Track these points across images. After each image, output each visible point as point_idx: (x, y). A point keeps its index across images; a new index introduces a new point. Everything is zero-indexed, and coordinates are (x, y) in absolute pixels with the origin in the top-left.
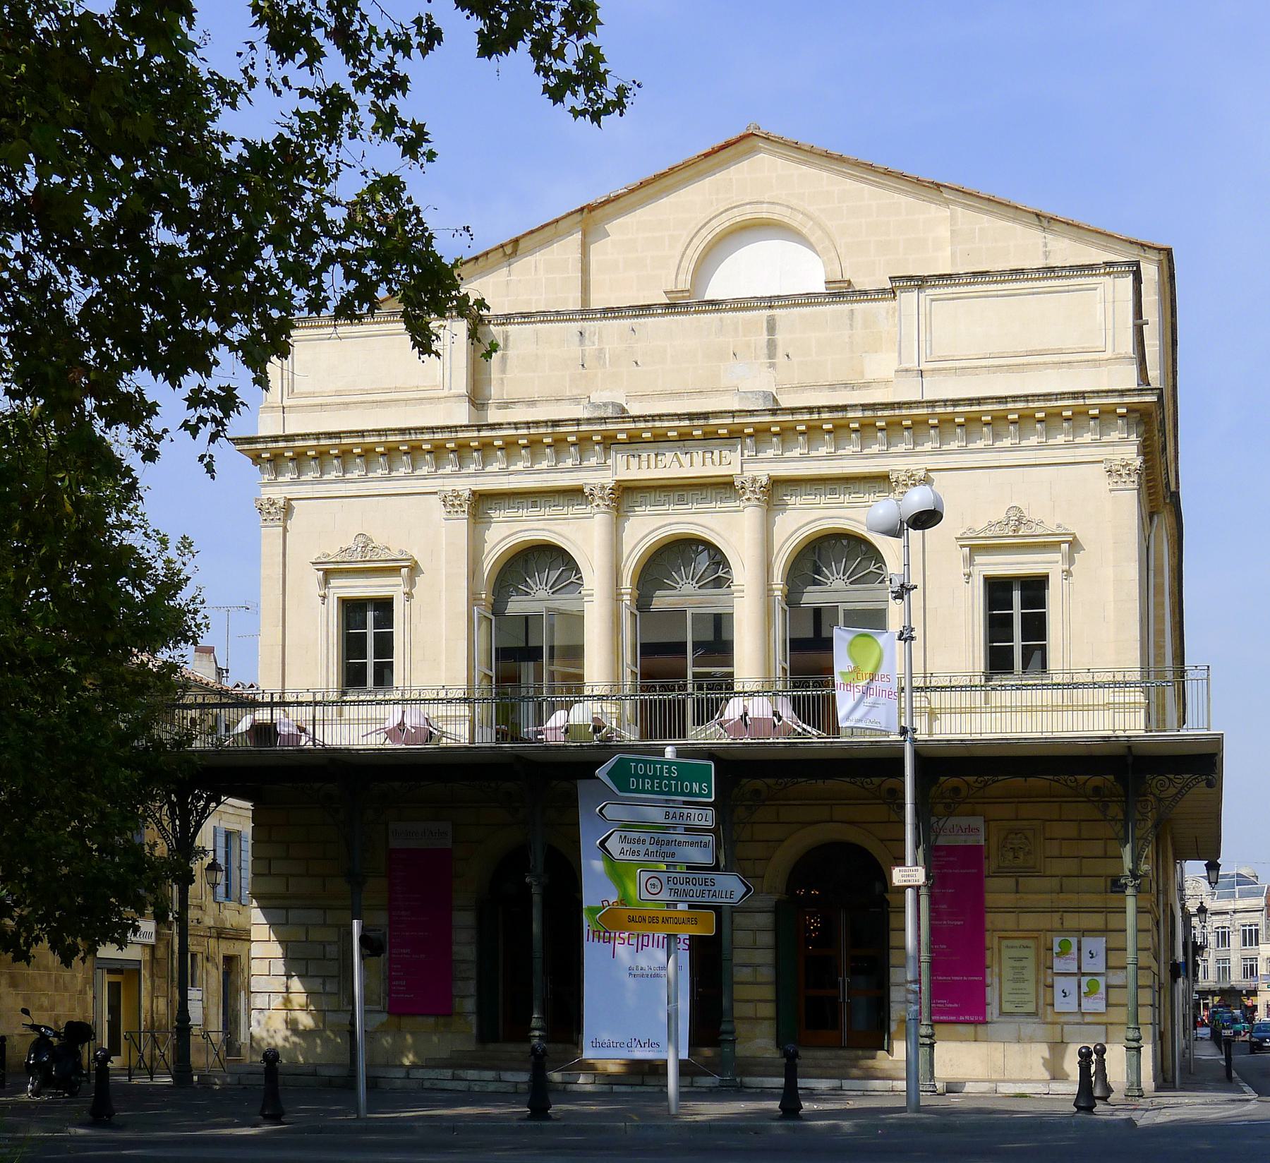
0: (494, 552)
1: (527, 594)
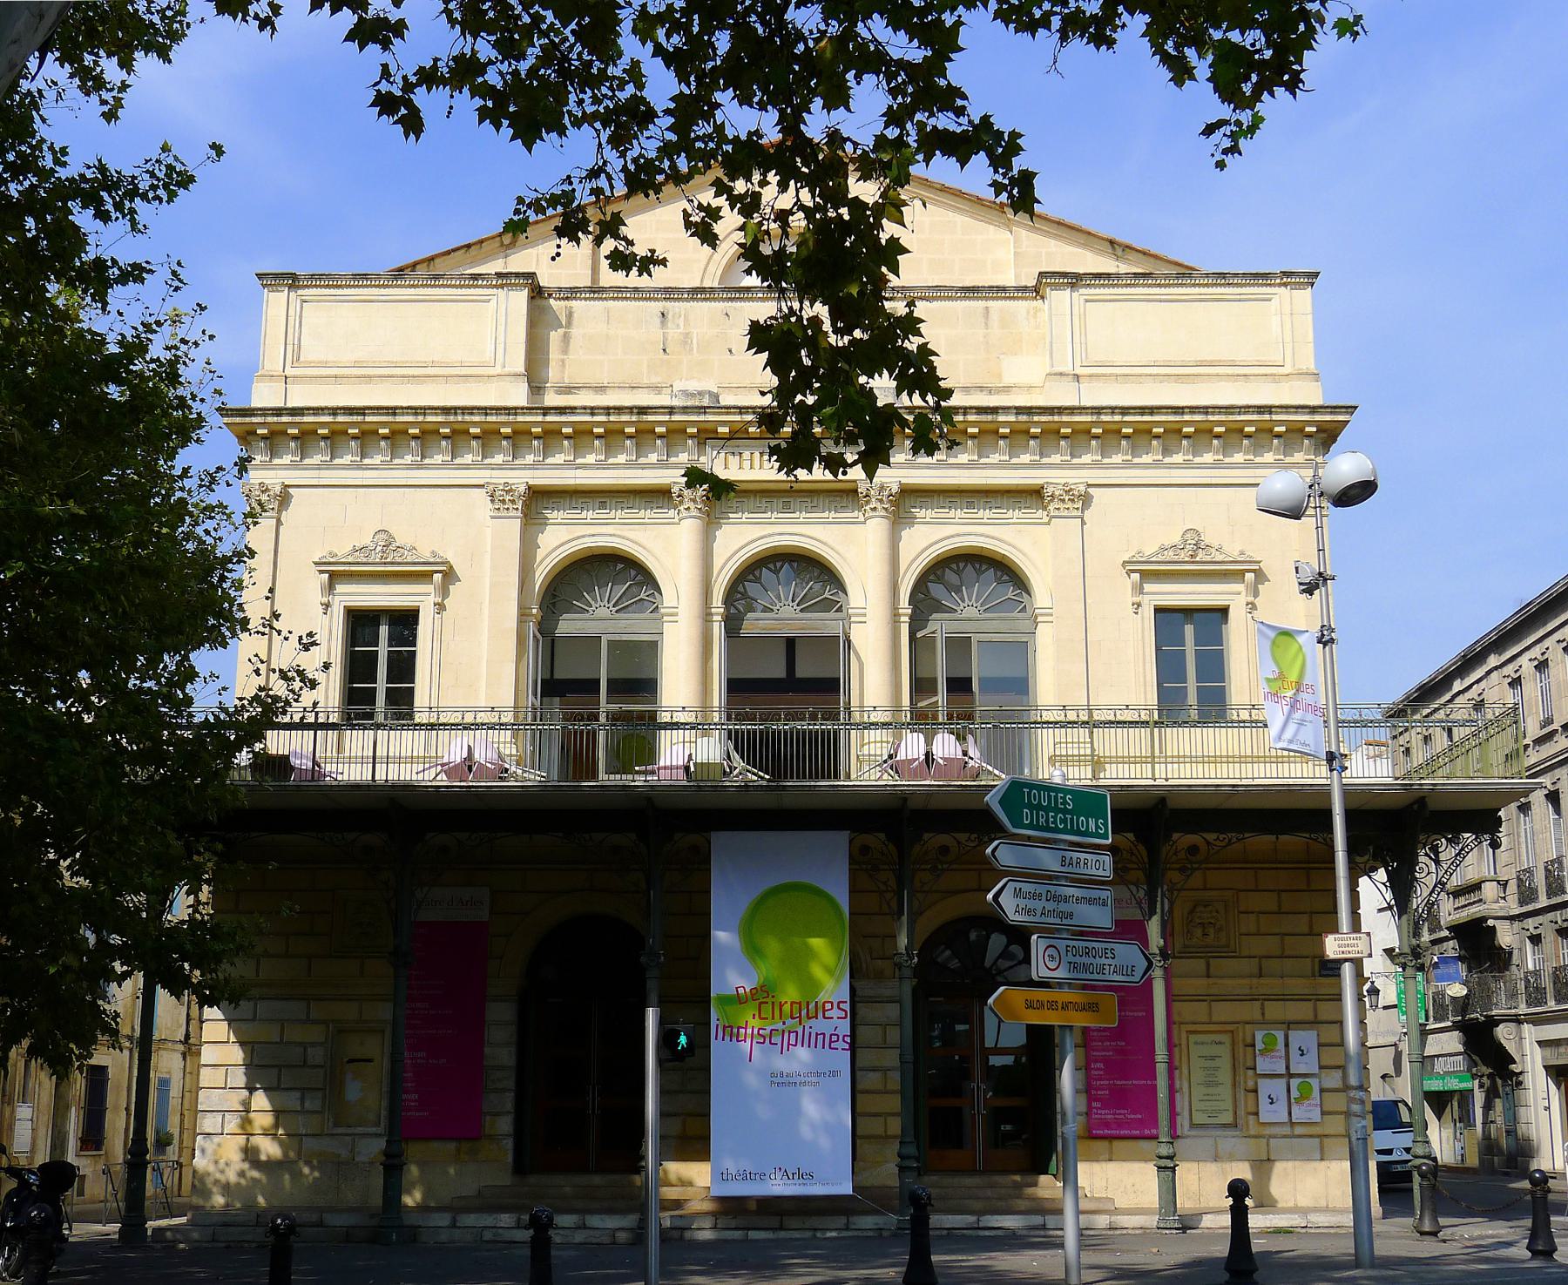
0: (548, 560)
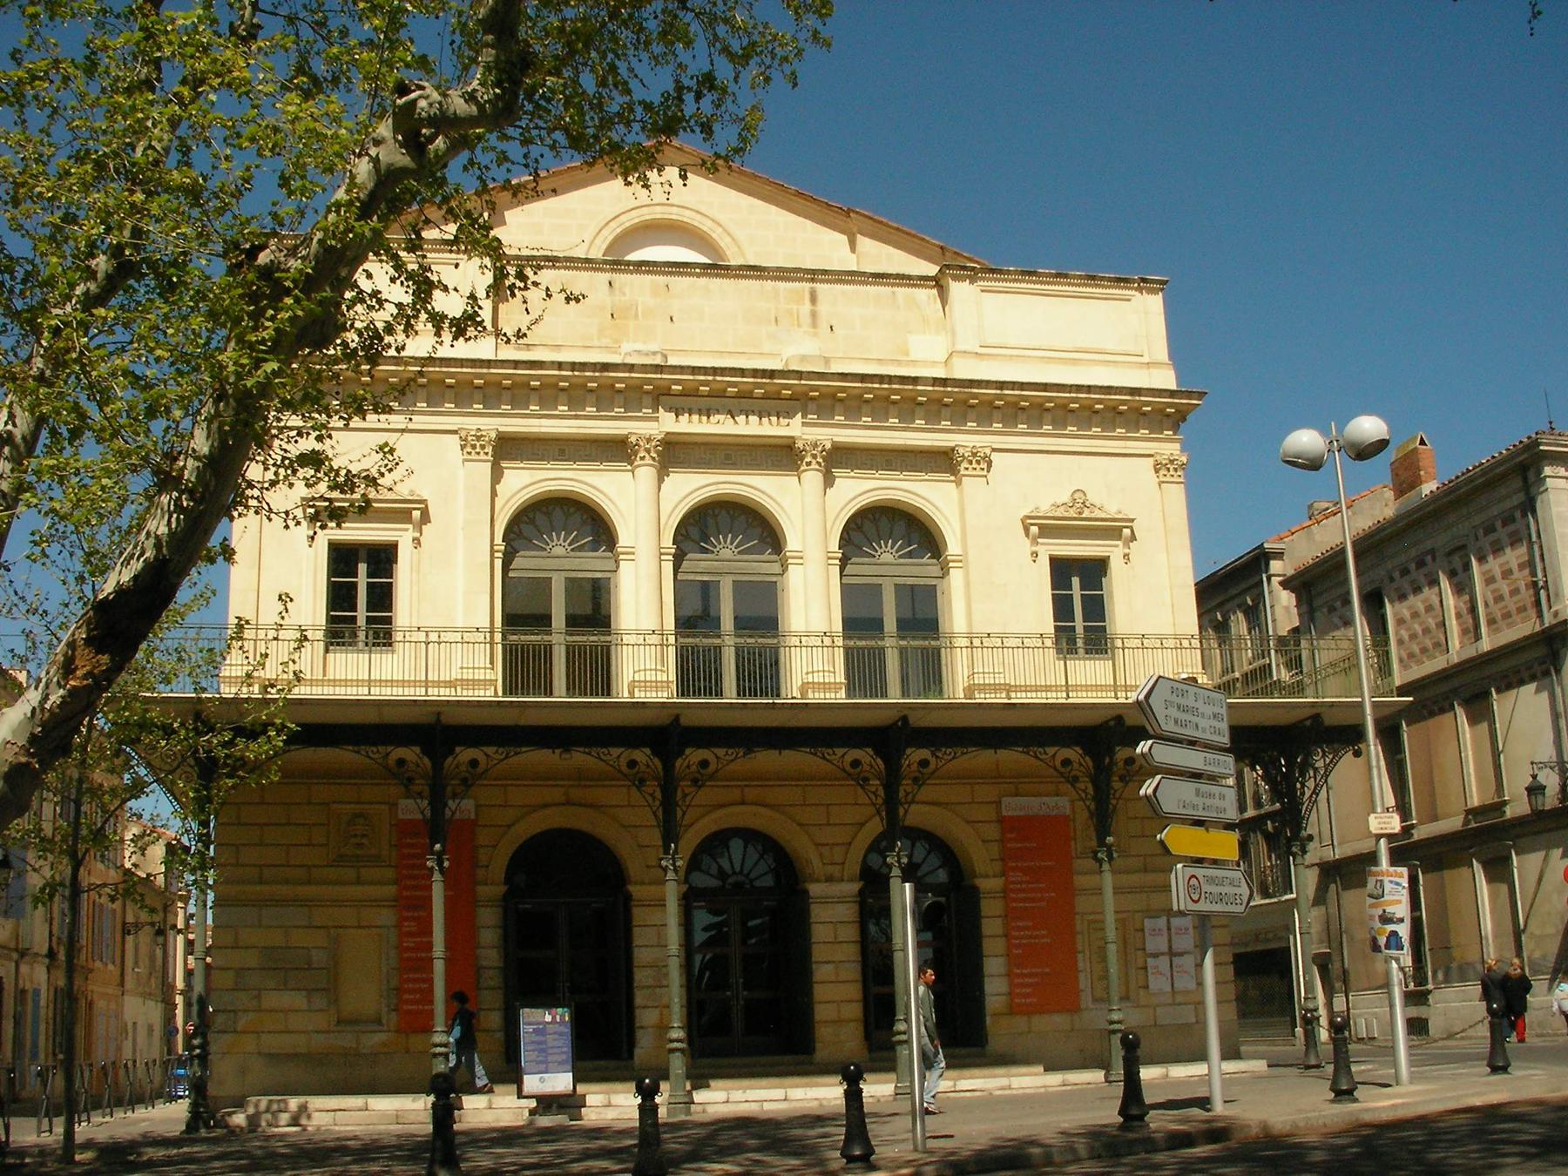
1: (706, 551)
